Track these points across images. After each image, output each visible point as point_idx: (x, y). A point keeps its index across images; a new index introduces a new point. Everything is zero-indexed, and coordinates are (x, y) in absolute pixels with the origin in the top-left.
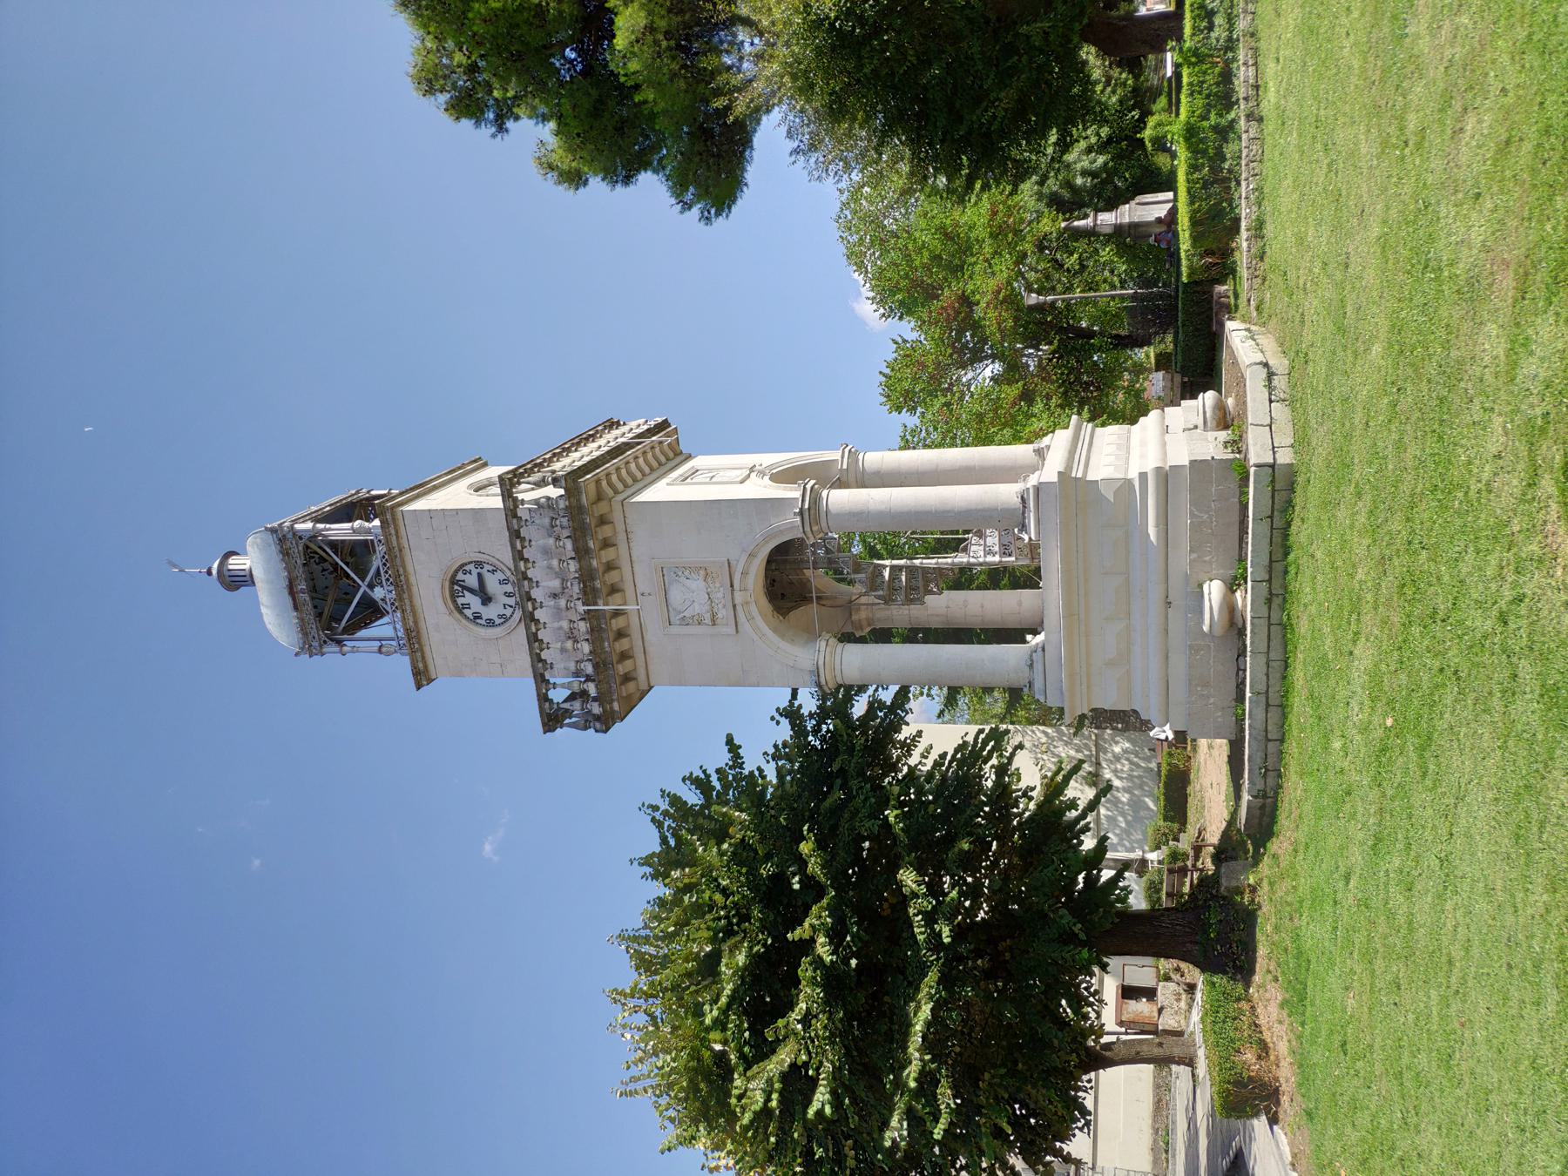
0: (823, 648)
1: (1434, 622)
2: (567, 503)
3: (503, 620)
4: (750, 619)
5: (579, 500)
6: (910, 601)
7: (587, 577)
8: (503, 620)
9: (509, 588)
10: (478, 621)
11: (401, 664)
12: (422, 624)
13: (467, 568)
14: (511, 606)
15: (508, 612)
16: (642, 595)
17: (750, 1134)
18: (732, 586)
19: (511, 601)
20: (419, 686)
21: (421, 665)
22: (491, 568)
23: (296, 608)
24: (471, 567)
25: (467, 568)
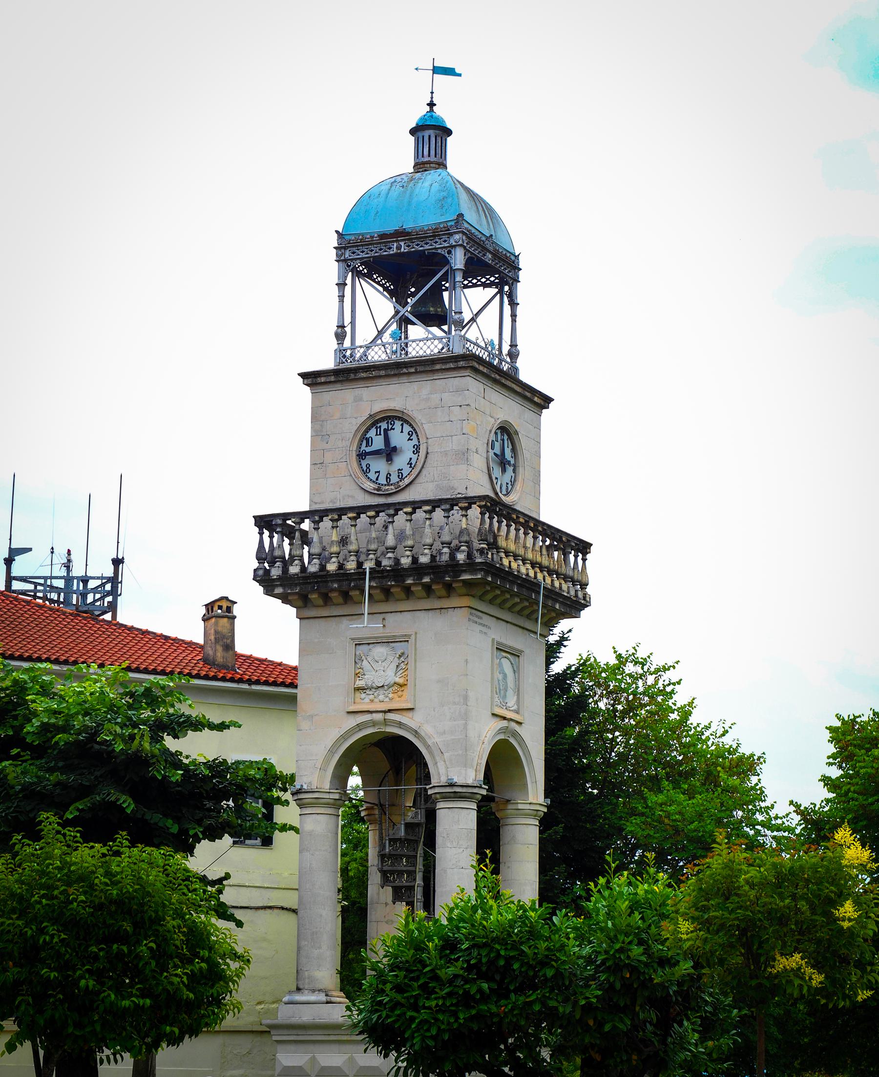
0: (332, 796)
1: (316, 933)
2: (461, 562)
3: (365, 469)
4: (360, 727)
5: (465, 571)
6: (384, 874)
7: (397, 572)
8: (365, 469)
9: (394, 479)
10: (365, 442)
11: (327, 362)
12: (361, 384)
13: (414, 437)
14: (377, 479)
15: (372, 475)
16: (384, 619)
17: (820, 1044)
18: (390, 711)
19: (382, 480)
20: (304, 376)
21: (323, 380)
22: (413, 462)
23: (383, 236)
24: (415, 442)
25: (414, 437)
